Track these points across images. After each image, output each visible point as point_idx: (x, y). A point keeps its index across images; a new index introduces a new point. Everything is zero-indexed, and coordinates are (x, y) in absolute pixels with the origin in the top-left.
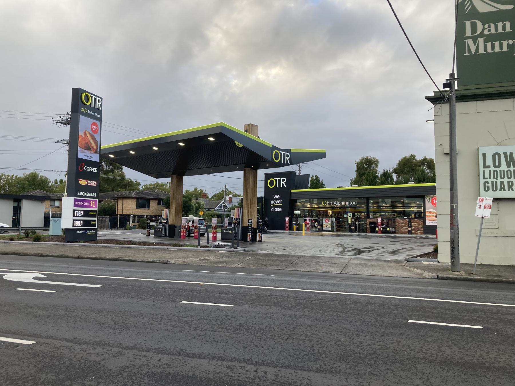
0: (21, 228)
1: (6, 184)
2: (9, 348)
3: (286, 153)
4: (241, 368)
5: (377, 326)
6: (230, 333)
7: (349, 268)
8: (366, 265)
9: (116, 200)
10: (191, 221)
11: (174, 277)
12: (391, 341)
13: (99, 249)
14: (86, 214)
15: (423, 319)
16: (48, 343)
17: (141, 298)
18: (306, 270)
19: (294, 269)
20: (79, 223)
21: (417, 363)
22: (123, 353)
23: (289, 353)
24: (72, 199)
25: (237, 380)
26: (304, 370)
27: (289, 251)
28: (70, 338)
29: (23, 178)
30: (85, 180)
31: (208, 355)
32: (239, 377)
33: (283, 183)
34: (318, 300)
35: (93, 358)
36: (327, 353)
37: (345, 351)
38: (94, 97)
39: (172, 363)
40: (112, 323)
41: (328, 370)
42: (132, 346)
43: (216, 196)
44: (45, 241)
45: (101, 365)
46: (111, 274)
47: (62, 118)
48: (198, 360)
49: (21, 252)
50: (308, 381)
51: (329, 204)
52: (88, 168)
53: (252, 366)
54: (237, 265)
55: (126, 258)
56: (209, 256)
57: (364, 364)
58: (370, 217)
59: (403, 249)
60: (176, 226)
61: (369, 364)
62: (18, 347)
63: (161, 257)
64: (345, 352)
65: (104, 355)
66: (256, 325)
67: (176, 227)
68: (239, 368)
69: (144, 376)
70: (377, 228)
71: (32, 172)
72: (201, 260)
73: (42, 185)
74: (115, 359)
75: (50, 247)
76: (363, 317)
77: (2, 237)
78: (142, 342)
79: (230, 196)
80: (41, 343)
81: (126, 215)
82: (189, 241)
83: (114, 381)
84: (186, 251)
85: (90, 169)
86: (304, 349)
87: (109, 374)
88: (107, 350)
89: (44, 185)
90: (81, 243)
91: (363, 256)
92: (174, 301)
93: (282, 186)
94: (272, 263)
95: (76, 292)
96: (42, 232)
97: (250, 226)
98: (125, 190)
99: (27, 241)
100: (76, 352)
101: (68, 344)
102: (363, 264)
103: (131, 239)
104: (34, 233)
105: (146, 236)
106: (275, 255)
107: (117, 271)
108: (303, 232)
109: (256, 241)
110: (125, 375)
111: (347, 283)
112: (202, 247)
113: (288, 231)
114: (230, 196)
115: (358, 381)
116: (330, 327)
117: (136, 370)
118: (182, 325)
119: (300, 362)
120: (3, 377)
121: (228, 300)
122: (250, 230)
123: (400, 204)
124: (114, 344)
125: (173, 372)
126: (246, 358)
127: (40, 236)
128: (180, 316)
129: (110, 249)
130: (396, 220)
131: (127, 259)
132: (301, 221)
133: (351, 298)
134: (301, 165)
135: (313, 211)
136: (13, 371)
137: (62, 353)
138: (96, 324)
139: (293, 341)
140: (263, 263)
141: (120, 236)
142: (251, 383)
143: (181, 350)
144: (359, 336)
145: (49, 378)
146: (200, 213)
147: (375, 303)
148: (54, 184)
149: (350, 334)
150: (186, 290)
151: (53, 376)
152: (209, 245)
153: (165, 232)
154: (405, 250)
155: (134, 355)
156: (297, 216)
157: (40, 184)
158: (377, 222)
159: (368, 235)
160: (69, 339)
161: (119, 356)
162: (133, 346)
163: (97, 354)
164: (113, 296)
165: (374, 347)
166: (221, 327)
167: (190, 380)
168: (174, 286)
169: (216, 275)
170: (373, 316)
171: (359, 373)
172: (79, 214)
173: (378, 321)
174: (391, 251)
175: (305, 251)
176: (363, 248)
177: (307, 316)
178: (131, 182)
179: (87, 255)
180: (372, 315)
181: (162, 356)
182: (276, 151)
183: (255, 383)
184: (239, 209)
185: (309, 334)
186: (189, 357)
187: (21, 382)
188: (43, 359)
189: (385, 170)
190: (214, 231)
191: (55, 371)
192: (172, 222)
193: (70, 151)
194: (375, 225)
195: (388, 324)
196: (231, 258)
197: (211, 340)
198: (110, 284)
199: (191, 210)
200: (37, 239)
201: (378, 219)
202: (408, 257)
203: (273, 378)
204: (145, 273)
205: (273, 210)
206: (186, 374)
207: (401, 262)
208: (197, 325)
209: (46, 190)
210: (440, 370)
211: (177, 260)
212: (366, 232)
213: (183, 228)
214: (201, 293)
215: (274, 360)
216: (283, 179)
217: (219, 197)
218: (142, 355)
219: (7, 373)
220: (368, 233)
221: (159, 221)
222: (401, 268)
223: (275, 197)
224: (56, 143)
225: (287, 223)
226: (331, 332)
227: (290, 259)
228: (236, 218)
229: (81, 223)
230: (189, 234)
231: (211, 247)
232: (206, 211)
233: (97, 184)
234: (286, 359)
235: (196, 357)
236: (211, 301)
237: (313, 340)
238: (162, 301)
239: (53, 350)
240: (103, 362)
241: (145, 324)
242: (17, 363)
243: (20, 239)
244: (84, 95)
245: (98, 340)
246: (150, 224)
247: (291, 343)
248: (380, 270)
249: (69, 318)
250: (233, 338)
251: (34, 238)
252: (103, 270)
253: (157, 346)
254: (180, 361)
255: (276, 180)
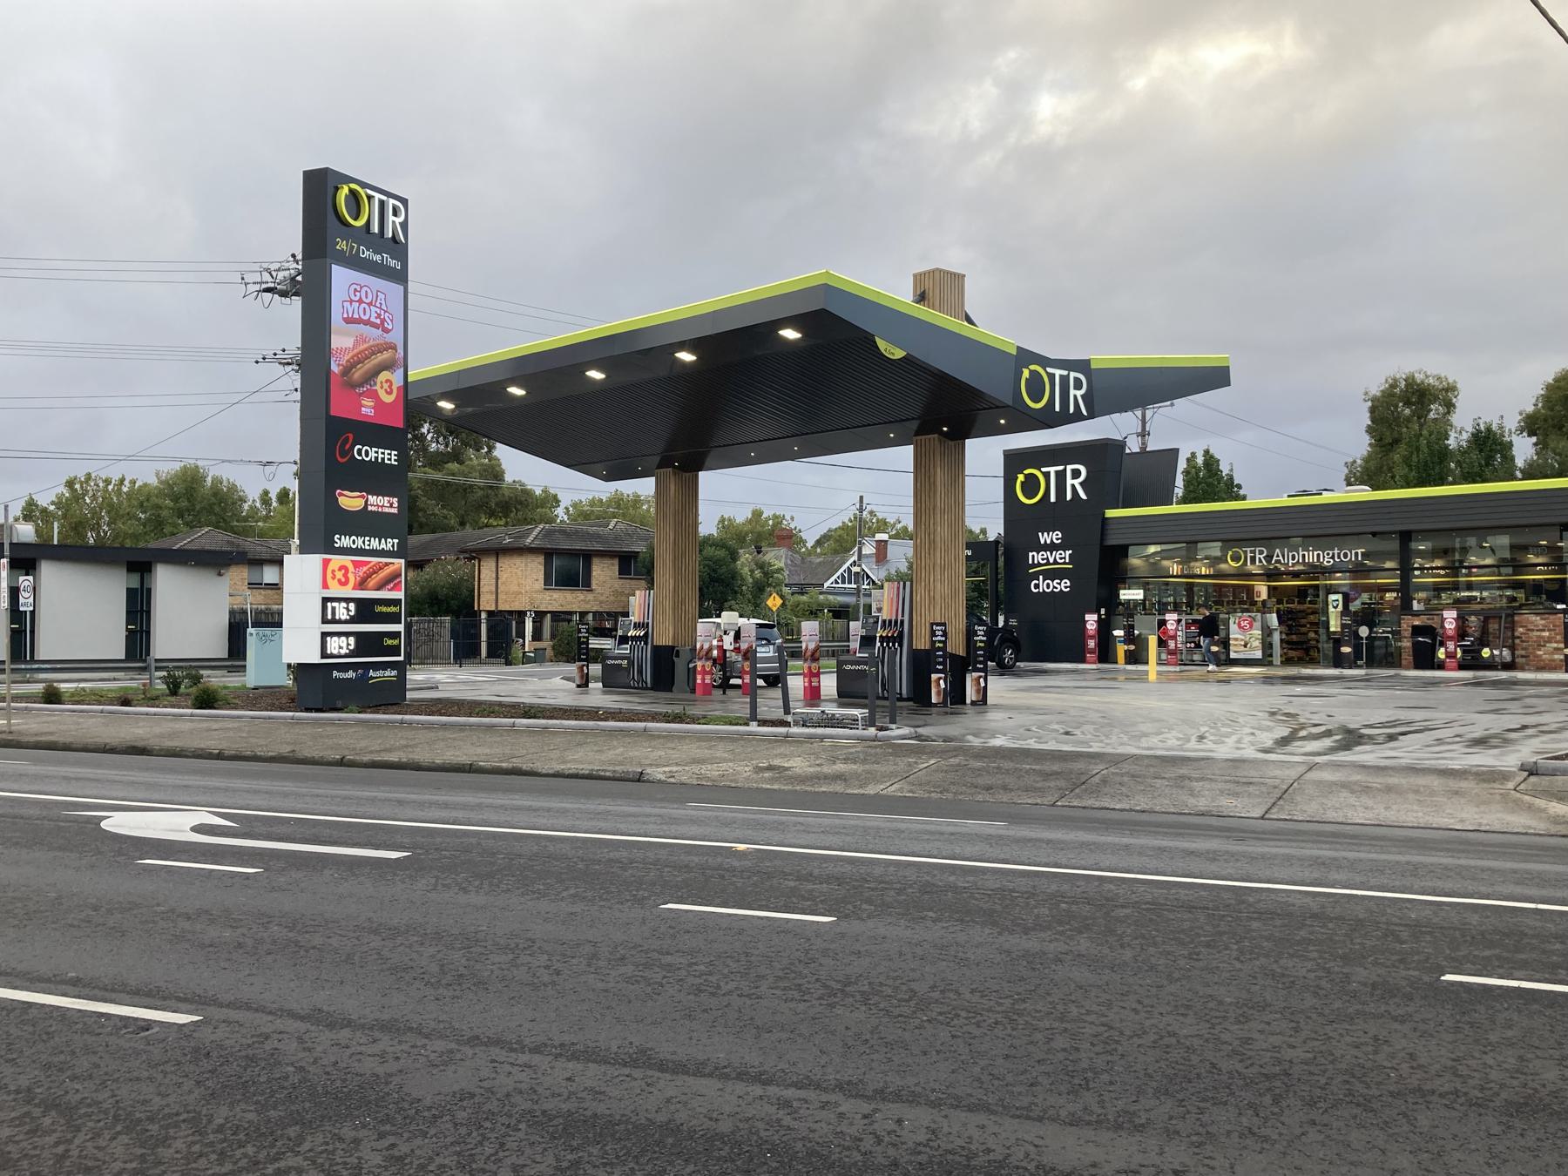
0: (153, 665)
1: (101, 509)
2: (123, 1032)
3: (1073, 375)
4: (823, 1108)
5: (1322, 992)
6: (809, 1004)
7: (1299, 799)
8: (1366, 789)
9: (474, 558)
10: (732, 634)
11: (655, 827)
12: (1355, 1039)
13: (410, 734)
14: (366, 611)
15: (1501, 971)
16: (237, 1022)
17: (533, 892)
18: (1136, 805)
19: (1089, 803)
20: (344, 645)
21: (1423, 1107)
22: (458, 1056)
23: (990, 1068)
24: (315, 560)
25: (803, 1139)
26: (1028, 1118)
27: (1080, 736)
28: (302, 1009)
29: (156, 488)
30: (358, 494)
31: (725, 1067)
32: (813, 1131)
33: (1073, 486)
34: (1136, 905)
35: (369, 1066)
36: (1121, 1069)
37: (1181, 1067)
38: (377, 196)
39: (608, 1086)
40: (434, 968)
41: (1108, 1119)
42: (488, 1037)
43: (830, 537)
44: (232, 709)
45: (391, 1086)
46: (444, 814)
47: (274, 275)
48: (690, 1080)
49: (154, 743)
50: (1032, 1148)
51: (1253, 560)
52: (367, 452)
53: (859, 1101)
54: (882, 787)
55: (501, 761)
56: (786, 756)
57: (1237, 1106)
58: (1416, 606)
59: (1524, 727)
60: (678, 651)
61: (1250, 1105)
62: (148, 1030)
63: (620, 758)
64: (1180, 1070)
65: (402, 1061)
66: (900, 981)
67: (678, 656)
68: (818, 1105)
69: (519, 1121)
70: (1442, 650)
71: (185, 466)
72: (758, 770)
73: (217, 509)
74: (434, 1072)
75: (247, 729)
76: (1283, 962)
77: (95, 694)
78: (520, 1026)
79: (880, 537)
80: (217, 1021)
81: (510, 612)
82: (723, 702)
83: (427, 1133)
84: (711, 739)
85: (372, 455)
86: (1046, 1057)
87: (414, 1111)
88: (412, 1047)
89: (224, 510)
90: (351, 712)
91: (1363, 755)
92: (641, 902)
93: (1069, 497)
94: (1010, 780)
95: (327, 872)
96: (223, 676)
97: (939, 649)
98: (506, 524)
99: (173, 706)
100: (319, 1049)
101: (295, 1025)
102: (1356, 783)
103: (527, 699)
104: (196, 680)
105: (574, 685)
106: (1026, 753)
107: (465, 807)
108: (1152, 668)
109: (964, 702)
110: (461, 1115)
111: (1267, 849)
112: (763, 723)
113: (1094, 666)
114: (880, 537)
115: (1198, 1154)
116: (1154, 990)
117: (496, 1103)
118: (654, 975)
119: (1020, 1093)
120: (106, 1112)
121: (822, 901)
122: (940, 664)
123: (1537, 555)
124: (434, 1030)
125: (608, 1112)
126: (847, 1078)
127: (215, 692)
128: (654, 950)
129: (448, 734)
130: (1516, 618)
131: (504, 765)
132: (1144, 626)
133: (1260, 901)
134: (1149, 413)
135: (1196, 589)
136: (133, 1096)
137: (276, 1049)
138: (382, 971)
139: (1014, 1033)
140: (980, 781)
141: (487, 686)
142: (848, 1149)
143: (643, 1052)
144: (1248, 1020)
145: (238, 1117)
146: (770, 603)
147: (1340, 918)
148: (258, 505)
149: (1218, 1014)
150: (686, 866)
151: (251, 1111)
152: (789, 719)
153: (640, 672)
154: (1530, 732)
155: (493, 1061)
156: (1131, 608)
157: (209, 509)
158: (1443, 627)
159: (1406, 678)
160: (300, 1011)
161: (445, 1064)
162: (491, 1036)
163: (382, 1056)
164: (444, 885)
165: (1289, 1054)
166: (781, 984)
167: (657, 1136)
168: (648, 854)
169: (801, 819)
170: (1321, 958)
171: (1210, 1129)
172: (342, 611)
173: (1333, 976)
174: (1476, 735)
175: (1143, 740)
176: (1367, 726)
177: (1084, 956)
178: (527, 493)
179: (371, 752)
180: (1315, 955)
181: (580, 1066)
182: (1033, 367)
183: (860, 1151)
184: (898, 588)
185: (1074, 1011)
186: (662, 1071)
187: (157, 1127)
188: (220, 1065)
189: (1481, 422)
190: (810, 668)
191: (255, 1098)
192: (663, 637)
193: (306, 389)
194: (1434, 639)
195: (1365, 985)
196: (864, 761)
197: (741, 1024)
198: (436, 849)
199: (736, 592)
200: (207, 700)
201: (1446, 614)
202: (1534, 760)
203: (922, 1137)
204: (557, 812)
205: (1037, 586)
206: (648, 1119)
207: (1504, 776)
208: (704, 977)
209: (232, 527)
210: (1496, 1129)
211: (675, 769)
212: (1399, 666)
213: (700, 659)
214: (734, 879)
215: (937, 1086)
216: (1073, 470)
217: (841, 541)
218: (518, 1062)
219: (117, 1102)
220: (1407, 668)
221: (620, 633)
222: (1498, 797)
223: (1045, 538)
224: (257, 362)
225: (1092, 637)
226: (1152, 1006)
227: (1079, 766)
228: (890, 621)
229: (348, 644)
230: (726, 679)
231: (796, 723)
232: (793, 594)
233: (398, 507)
234: (976, 1084)
235: (687, 1073)
236: (764, 903)
237: (1084, 1031)
238: (602, 903)
239: (250, 1042)
240: (396, 1080)
241: (538, 974)
242: (146, 1074)
243: (153, 700)
244: (345, 191)
245: (386, 1016)
246: (587, 644)
247: (1003, 1039)
248: (1415, 808)
249: (302, 953)
250: (813, 1019)
251: (196, 698)
252: (421, 805)
253: (567, 1038)
254: (634, 1083)
255: (1047, 475)
